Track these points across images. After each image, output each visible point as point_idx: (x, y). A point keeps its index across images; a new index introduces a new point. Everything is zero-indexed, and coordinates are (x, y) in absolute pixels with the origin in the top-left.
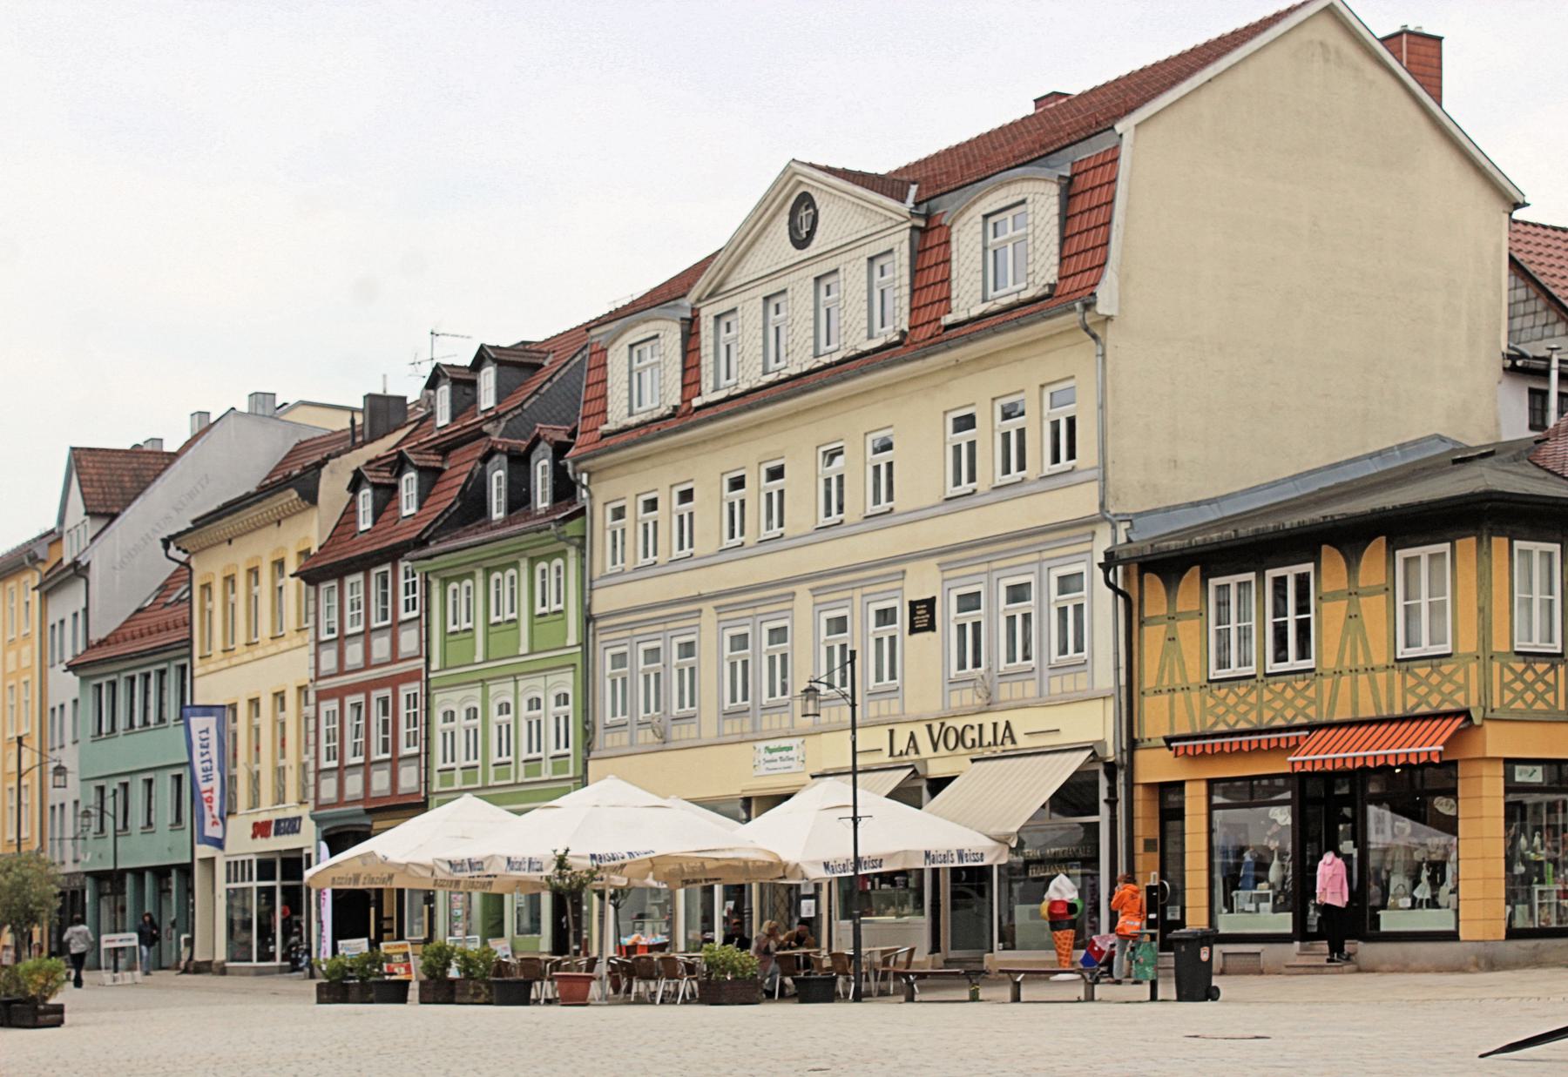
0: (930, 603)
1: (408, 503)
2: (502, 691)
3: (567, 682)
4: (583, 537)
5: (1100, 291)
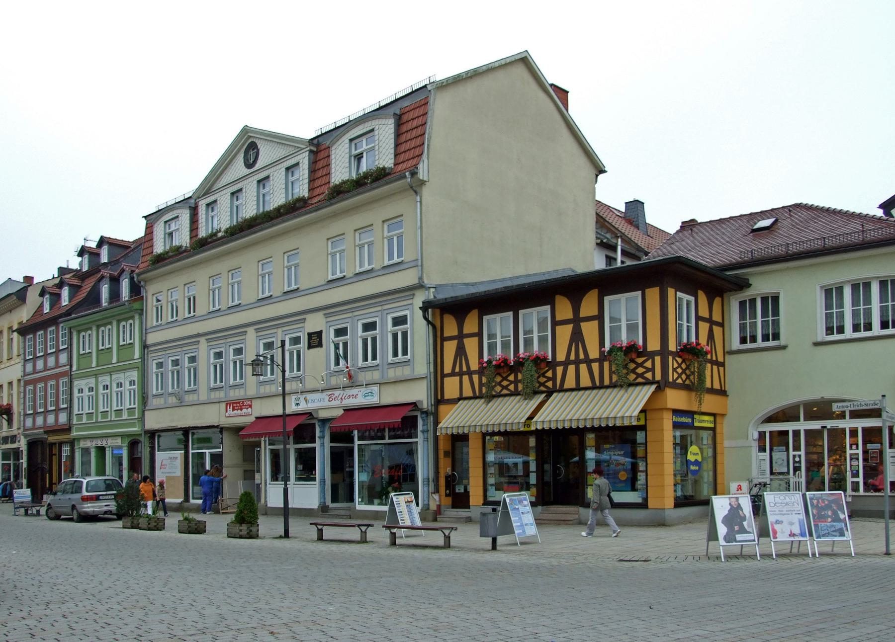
0: (319, 334)
1: (65, 300)
2: (105, 379)
3: (134, 375)
4: (142, 310)
5: (420, 166)
